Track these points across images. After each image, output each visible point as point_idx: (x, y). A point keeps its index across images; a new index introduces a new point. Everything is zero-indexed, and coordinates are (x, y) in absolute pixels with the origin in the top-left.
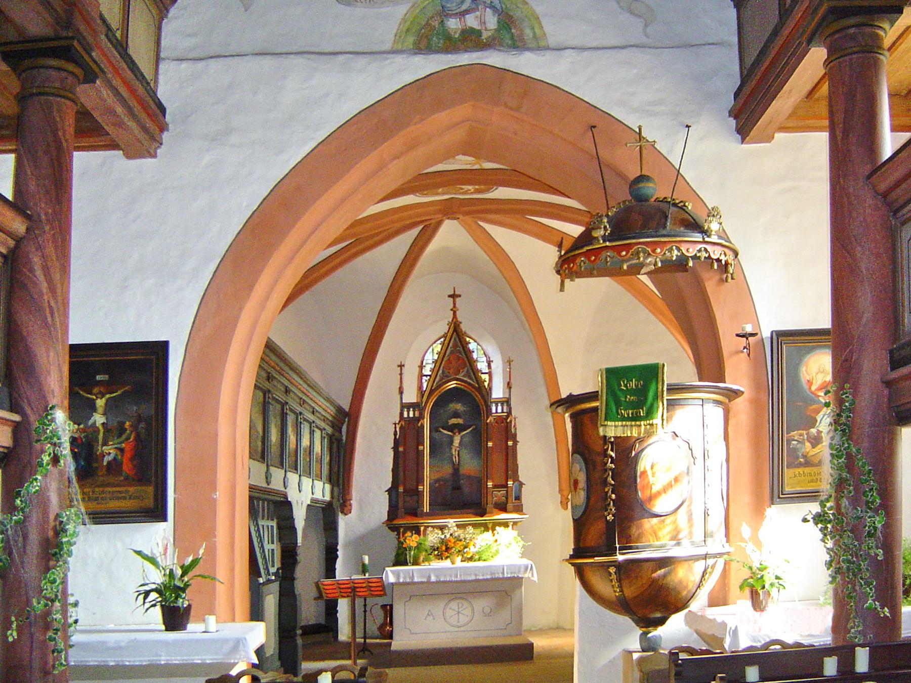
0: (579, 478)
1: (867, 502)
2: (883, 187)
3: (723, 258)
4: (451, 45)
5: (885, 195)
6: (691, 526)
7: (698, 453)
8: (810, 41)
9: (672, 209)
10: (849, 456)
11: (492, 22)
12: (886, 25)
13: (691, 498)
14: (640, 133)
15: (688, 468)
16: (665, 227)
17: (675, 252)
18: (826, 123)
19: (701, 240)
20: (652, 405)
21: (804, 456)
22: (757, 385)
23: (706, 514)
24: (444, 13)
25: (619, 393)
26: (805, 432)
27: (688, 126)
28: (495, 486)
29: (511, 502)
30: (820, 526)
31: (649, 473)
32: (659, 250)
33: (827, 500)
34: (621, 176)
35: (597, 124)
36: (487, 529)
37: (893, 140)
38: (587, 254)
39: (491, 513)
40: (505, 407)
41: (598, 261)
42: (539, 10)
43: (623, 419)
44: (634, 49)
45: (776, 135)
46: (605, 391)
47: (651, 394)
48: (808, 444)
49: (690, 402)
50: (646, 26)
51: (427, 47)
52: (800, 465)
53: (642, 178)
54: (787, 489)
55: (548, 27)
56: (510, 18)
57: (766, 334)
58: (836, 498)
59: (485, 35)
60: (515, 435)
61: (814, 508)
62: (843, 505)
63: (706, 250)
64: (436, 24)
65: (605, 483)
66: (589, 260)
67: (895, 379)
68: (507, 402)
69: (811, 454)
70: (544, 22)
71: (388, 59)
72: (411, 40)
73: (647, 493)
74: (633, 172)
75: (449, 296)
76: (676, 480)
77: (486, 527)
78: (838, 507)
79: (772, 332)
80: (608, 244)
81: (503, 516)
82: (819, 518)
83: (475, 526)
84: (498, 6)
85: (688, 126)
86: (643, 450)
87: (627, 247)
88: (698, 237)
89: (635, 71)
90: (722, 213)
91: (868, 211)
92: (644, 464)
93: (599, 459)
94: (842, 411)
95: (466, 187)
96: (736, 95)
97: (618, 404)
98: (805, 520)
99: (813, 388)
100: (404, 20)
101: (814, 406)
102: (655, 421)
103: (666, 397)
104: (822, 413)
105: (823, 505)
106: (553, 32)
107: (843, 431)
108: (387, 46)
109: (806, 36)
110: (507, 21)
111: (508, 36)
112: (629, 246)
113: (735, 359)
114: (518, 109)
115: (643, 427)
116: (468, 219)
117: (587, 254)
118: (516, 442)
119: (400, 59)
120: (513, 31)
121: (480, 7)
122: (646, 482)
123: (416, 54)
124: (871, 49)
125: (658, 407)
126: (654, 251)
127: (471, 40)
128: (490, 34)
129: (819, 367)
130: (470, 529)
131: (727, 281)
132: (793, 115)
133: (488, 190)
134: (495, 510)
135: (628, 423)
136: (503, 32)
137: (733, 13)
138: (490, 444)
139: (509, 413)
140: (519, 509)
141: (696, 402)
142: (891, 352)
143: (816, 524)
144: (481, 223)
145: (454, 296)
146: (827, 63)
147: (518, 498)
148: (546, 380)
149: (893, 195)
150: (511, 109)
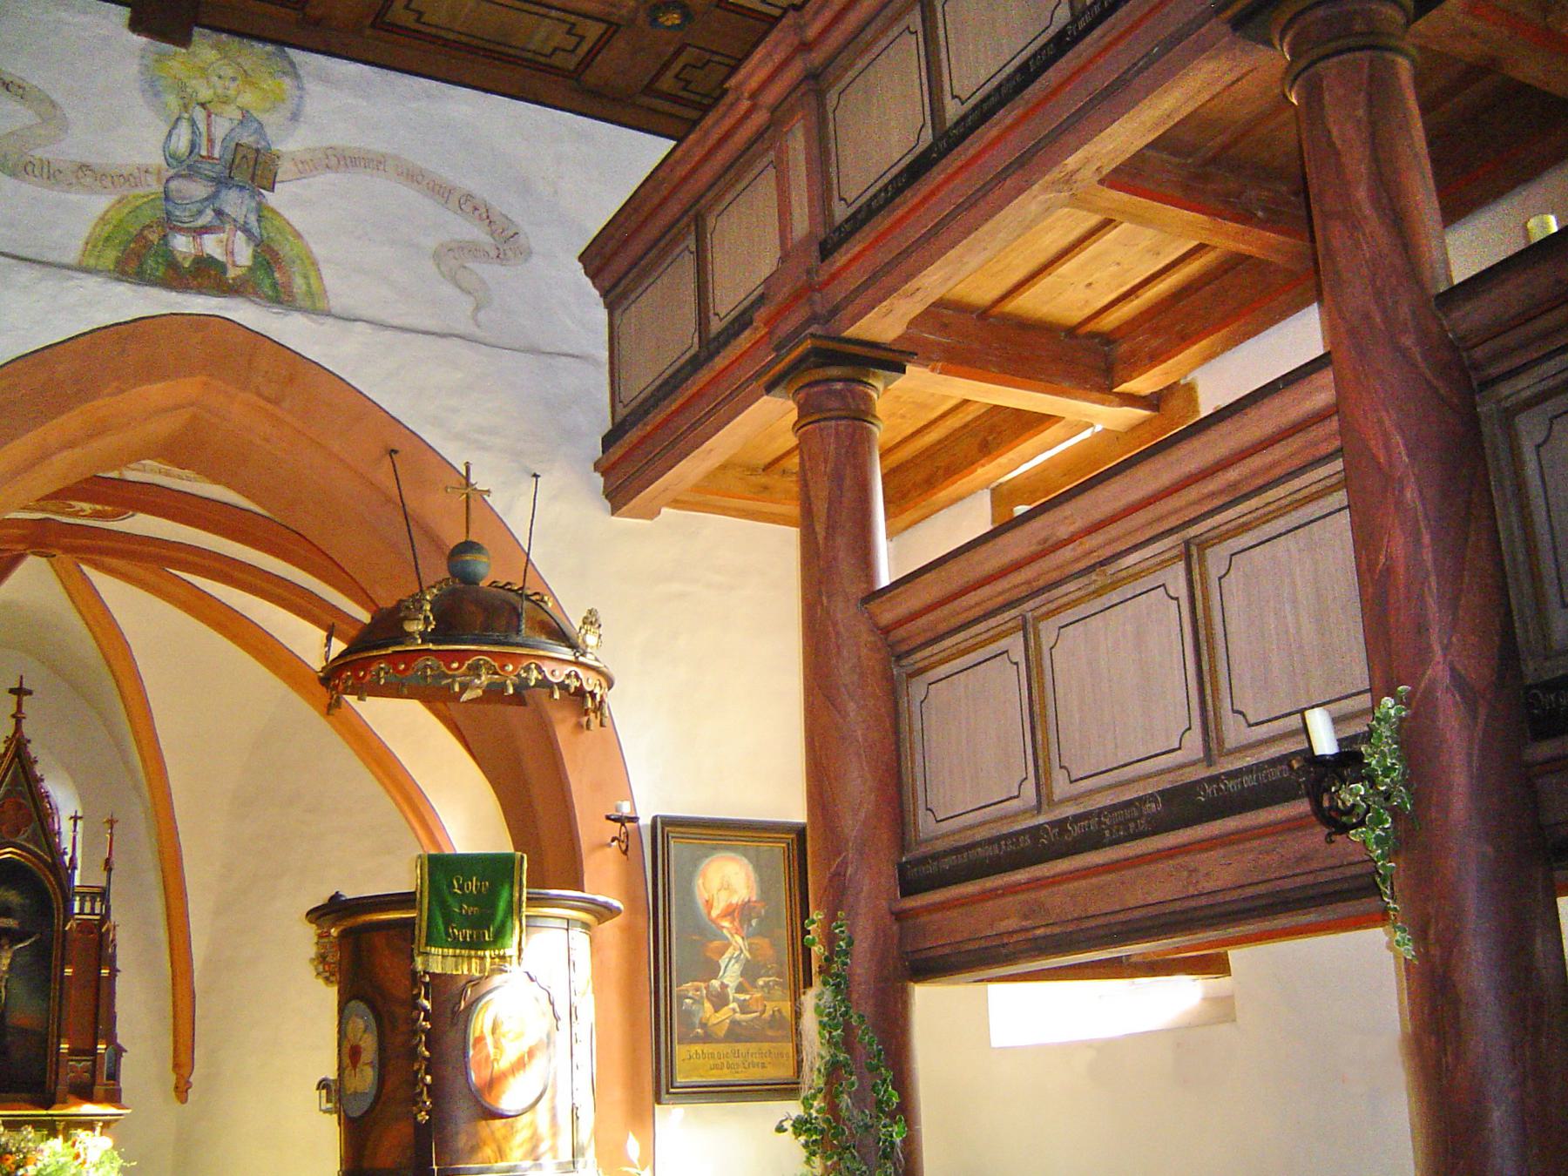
0: (362, 1044)
1: (880, 1102)
2: (886, 618)
3: (597, 690)
4: (181, 277)
5: (886, 631)
6: (555, 1135)
7: (563, 1012)
8: (769, 389)
9: (526, 604)
10: (847, 1027)
11: (244, 254)
12: (880, 385)
13: (554, 1085)
14: (467, 478)
15: (548, 1036)
16: (518, 632)
17: (535, 674)
18: (794, 509)
19: (572, 658)
20: (503, 924)
21: (704, 1025)
22: (631, 898)
23: (575, 1117)
24: (169, 224)
25: (450, 899)
26: (702, 985)
27: (536, 476)
28: (72, 1052)
29: (100, 1082)
30: (802, 1139)
31: (489, 1040)
32: (510, 668)
33: (814, 1097)
34: (436, 541)
35: (399, 448)
36: (53, 1133)
37: (894, 558)
38: (392, 659)
39: (64, 1102)
40: (98, 905)
41: (410, 672)
42: (319, 251)
43: (456, 944)
44: (459, 341)
45: (665, 510)
46: (426, 894)
47: (502, 905)
48: (707, 1005)
49: (539, 922)
50: (478, 309)
51: (137, 274)
52: (698, 1040)
53: (469, 546)
54: (680, 1079)
55: (331, 278)
56: (274, 254)
57: (645, 820)
58: (829, 1092)
59: (232, 273)
60: (114, 956)
61: (794, 1109)
62: (843, 1105)
63: (577, 676)
64: (154, 237)
65: (413, 1054)
66: (395, 668)
67: (913, 909)
68: (103, 894)
69: (714, 1021)
70: (327, 273)
71: (72, 278)
72: (111, 255)
73: (486, 1074)
74: (454, 537)
75: (12, 691)
76: (531, 1053)
77: (50, 1129)
78: (833, 1107)
79: (655, 819)
80: (431, 646)
81: (88, 1108)
82: (801, 1126)
83: (37, 1124)
84: (256, 231)
85: (536, 476)
86: (478, 1000)
87: (462, 656)
88: (567, 654)
89: (460, 375)
90: (602, 621)
91: (864, 651)
92: (481, 1023)
93: (400, 1011)
94: (832, 952)
95: (79, 505)
96: (608, 441)
97: (448, 923)
98: (780, 1129)
99: (714, 913)
100: (103, 219)
101: (716, 943)
102: (508, 952)
103: (525, 911)
104: (727, 955)
105: (807, 1104)
106: (339, 289)
107: (837, 986)
108: (72, 257)
109: (765, 379)
110: (268, 258)
111: (268, 282)
112: (462, 656)
113: (599, 855)
114: (276, 402)
115: (488, 960)
116: (67, 558)
117: (392, 659)
118: (114, 971)
119: (92, 283)
120: (277, 275)
121: (227, 227)
122: (484, 1054)
123: (118, 280)
124: (861, 415)
125: (513, 929)
126: (503, 667)
127: (206, 275)
128: (239, 272)
129: (727, 881)
130: (29, 1132)
131: (588, 727)
132: (698, 488)
133: (114, 516)
134: (71, 1099)
135: (465, 952)
136: (260, 274)
137: (603, 315)
138: (68, 971)
139: (105, 917)
140: (113, 1097)
141: (558, 923)
142: (902, 869)
143: (797, 1134)
144: (85, 568)
145: (19, 692)
146: (797, 427)
147: (114, 1075)
148: (161, 860)
149: (901, 633)
150: (268, 400)
